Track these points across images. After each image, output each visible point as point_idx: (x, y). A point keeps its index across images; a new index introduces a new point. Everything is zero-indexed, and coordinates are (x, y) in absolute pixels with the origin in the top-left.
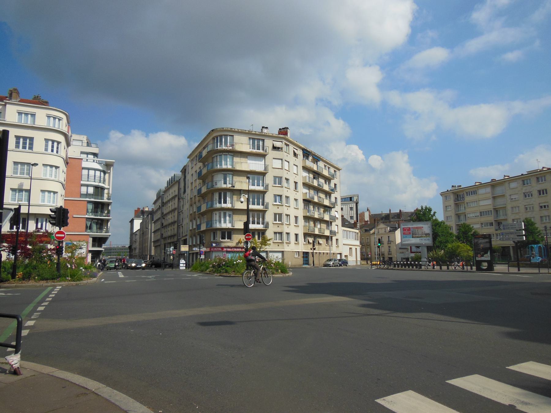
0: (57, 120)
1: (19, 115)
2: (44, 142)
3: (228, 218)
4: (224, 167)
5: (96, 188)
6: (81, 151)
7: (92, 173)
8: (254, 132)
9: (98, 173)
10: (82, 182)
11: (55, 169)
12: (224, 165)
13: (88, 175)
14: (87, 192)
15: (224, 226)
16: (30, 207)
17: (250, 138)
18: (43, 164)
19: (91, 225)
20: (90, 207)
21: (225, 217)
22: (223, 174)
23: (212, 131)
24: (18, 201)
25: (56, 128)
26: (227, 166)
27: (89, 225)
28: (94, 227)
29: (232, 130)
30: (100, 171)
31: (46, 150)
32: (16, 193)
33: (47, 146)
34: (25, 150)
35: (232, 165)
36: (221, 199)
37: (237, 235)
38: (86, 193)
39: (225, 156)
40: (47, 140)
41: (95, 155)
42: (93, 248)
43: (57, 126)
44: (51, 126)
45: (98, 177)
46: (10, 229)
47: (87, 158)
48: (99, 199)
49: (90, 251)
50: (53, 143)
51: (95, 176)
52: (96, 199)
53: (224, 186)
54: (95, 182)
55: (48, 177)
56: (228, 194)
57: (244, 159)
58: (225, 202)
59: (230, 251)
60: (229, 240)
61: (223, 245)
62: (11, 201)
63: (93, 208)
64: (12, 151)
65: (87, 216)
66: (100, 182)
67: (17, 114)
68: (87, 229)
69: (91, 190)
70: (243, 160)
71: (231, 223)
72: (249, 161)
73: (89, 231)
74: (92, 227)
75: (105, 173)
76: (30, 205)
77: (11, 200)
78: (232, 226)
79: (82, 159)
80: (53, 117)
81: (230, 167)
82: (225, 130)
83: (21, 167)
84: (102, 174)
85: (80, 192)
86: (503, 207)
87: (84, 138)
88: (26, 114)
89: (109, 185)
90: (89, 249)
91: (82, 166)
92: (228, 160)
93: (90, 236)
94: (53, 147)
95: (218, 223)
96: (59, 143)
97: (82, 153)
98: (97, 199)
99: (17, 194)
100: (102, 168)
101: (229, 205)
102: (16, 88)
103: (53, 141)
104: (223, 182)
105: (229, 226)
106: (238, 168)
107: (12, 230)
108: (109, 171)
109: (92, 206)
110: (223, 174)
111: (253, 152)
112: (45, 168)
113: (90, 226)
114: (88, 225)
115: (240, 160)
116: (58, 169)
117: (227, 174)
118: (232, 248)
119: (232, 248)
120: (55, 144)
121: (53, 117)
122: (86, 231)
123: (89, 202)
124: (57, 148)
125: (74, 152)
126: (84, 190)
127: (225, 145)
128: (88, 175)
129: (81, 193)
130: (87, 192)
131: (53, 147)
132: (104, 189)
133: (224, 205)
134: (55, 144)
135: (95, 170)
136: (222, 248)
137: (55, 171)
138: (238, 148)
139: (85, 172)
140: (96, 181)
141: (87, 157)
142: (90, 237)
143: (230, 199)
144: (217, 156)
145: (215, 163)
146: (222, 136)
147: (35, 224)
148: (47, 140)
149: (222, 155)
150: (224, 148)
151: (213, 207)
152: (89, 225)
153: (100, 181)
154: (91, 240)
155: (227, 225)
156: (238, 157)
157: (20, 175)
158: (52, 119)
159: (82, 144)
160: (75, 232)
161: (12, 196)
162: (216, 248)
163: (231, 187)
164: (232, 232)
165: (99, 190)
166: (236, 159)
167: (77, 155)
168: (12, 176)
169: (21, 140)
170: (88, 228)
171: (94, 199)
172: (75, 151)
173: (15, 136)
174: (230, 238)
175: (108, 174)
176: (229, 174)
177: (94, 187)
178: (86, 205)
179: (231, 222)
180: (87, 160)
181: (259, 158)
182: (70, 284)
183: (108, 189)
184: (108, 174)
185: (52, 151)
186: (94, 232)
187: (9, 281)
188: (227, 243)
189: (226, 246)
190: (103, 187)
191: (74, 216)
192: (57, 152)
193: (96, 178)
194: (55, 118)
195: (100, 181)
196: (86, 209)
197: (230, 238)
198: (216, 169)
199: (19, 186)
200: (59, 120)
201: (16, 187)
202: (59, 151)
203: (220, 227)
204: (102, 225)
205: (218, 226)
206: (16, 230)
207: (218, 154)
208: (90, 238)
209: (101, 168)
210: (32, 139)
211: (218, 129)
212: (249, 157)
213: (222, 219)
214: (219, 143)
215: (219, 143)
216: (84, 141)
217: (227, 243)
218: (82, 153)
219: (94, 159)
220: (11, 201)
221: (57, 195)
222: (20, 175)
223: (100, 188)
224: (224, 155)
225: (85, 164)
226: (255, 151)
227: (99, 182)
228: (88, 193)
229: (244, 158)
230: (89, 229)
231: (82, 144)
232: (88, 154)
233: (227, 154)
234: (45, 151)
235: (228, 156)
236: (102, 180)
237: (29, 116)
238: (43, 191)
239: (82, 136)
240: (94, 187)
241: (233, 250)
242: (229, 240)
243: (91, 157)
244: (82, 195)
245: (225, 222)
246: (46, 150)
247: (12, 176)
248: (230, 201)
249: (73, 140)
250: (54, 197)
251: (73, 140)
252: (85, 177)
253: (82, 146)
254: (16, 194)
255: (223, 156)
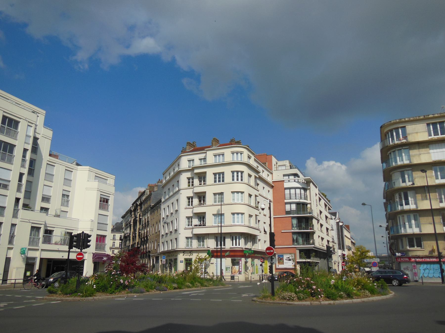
0: (239, 154)
1: (215, 157)
2: (213, 176)
3: (413, 222)
4: (399, 163)
5: (298, 204)
6: (283, 175)
7: (293, 191)
8: (432, 116)
9: (298, 191)
10: (286, 201)
11: (241, 194)
12: (400, 161)
13: (290, 194)
14: (291, 209)
15: (409, 231)
16: (222, 227)
17: (428, 125)
18: (232, 192)
19: (297, 238)
20: (295, 222)
21: (410, 222)
22: (400, 171)
23: (381, 127)
24: (218, 224)
25: (239, 160)
26: (403, 162)
27: (295, 238)
28: (300, 240)
29: (401, 120)
30: (300, 188)
31: (233, 180)
32: (216, 217)
33: (233, 176)
34: (216, 183)
35: (410, 160)
36: (402, 201)
37: (429, 242)
38: (290, 210)
39: (399, 151)
40: (233, 172)
41: (296, 175)
42: (300, 259)
43: (239, 159)
44: (235, 160)
45: (298, 194)
46: (216, 246)
47: (289, 179)
48: (302, 214)
49: (298, 263)
50: (238, 174)
51: (296, 194)
52: (298, 215)
53: (403, 185)
54: (296, 199)
55: (236, 201)
56: (410, 194)
57: (424, 149)
58: (407, 203)
59: (420, 262)
60: (419, 249)
61: (411, 254)
62: (214, 224)
63: (297, 223)
64: (212, 185)
65: (292, 231)
66: (301, 199)
67: (214, 157)
68: (294, 242)
69: (294, 207)
70: (423, 151)
71: (419, 227)
72: (431, 151)
73: (295, 243)
74: (298, 240)
75: (305, 190)
76: (222, 226)
77: (233, 222)
78: (421, 231)
79: (284, 181)
80: (236, 153)
81: (406, 162)
82: (393, 123)
83: (218, 196)
84: (303, 191)
85: (285, 209)
86: (28, 191)
87: (287, 163)
88: (219, 155)
89: (311, 200)
90: (297, 261)
91: (285, 187)
92: (403, 154)
93: (297, 249)
94: (238, 176)
95: (402, 229)
96: (242, 172)
97: (284, 175)
98: (300, 214)
99: (217, 218)
100: (301, 186)
101: (412, 206)
102: (214, 138)
103: (238, 172)
104: (401, 180)
105: (416, 231)
106: (416, 161)
107: (217, 247)
108: (309, 188)
109: (296, 221)
110: (400, 171)
111: (434, 139)
112: (238, 195)
113: (296, 240)
114: (294, 238)
115: (419, 151)
116: (243, 194)
117: (404, 171)
118: (422, 258)
119: (422, 258)
120: (240, 174)
121: (236, 153)
122: (293, 244)
123: (293, 218)
124: (242, 177)
125: (278, 176)
126: (288, 207)
127: (398, 139)
128: (290, 194)
129: (286, 210)
130: (291, 209)
131: (238, 176)
132: (307, 205)
133: (406, 207)
134: (240, 174)
135: (295, 188)
136: (410, 258)
137: (241, 196)
138: (412, 138)
139: (287, 192)
140: (297, 198)
141: (289, 178)
142: (297, 249)
143: (412, 199)
144: (390, 153)
145: (390, 160)
146: (393, 130)
147: (232, 242)
148: (233, 172)
149: (395, 151)
150: (396, 142)
151: (396, 210)
152: (295, 239)
153: (301, 197)
154: (298, 252)
155: (413, 230)
156: (416, 149)
157: (218, 203)
158: (235, 154)
159: (277, 168)
160: (284, 245)
161: (214, 220)
162: (402, 258)
163: (412, 184)
164: (422, 238)
165: (302, 206)
166: (413, 152)
167: (281, 178)
168: (213, 204)
169: (235, 174)
170: (294, 241)
171: (297, 215)
172: (279, 175)
173: (231, 171)
174: (419, 245)
175: (309, 190)
176: (406, 170)
177: (295, 203)
178: (291, 221)
179: (418, 226)
180: (289, 181)
181: (434, 145)
182: (74, 299)
183: (310, 204)
184: (309, 190)
185: (238, 180)
186: (301, 245)
187: (372, 283)
188: (417, 251)
189: (413, 256)
190: (304, 203)
191: (282, 231)
192: (242, 180)
193: (297, 196)
194: (237, 153)
195: (301, 197)
196: (291, 225)
197: (419, 245)
198: (392, 167)
199: (217, 212)
200: (241, 154)
201: (216, 213)
202: (243, 179)
203: (405, 233)
204: (309, 238)
205: (403, 231)
206: (220, 247)
207: (391, 151)
208: (297, 250)
209: (300, 186)
210: (223, 173)
211: (385, 125)
212: (431, 146)
213: (407, 224)
214: (390, 139)
215: (390, 139)
216: (287, 165)
217: (416, 252)
218: (284, 175)
219: (295, 179)
220: (214, 224)
221: (244, 216)
222: (218, 203)
223: (301, 204)
224: (398, 150)
225: (286, 185)
226: (433, 137)
227: (300, 198)
228: (292, 210)
229: (424, 148)
230: (296, 242)
231: (277, 168)
232: (289, 175)
233: (401, 148)
234: (232, 181)
235: (403, 150)
236: (303, 196)
237: (221, 156)
238: (233, 214)
239: (285, 161)
240: (296, 204)
241: (425, 260)
242: (420, 248)
243: (292, 177)
244: (288, 213)
245: (410, 227)
246: (233, 180)
247: (213, 204)
248: (413, 202)
249: (279, 166)
250: (242, 218)
251: (279, 166)
252: (287, 196)
253: (277, 170)
254: (216, 218)
255: (397, 152)
